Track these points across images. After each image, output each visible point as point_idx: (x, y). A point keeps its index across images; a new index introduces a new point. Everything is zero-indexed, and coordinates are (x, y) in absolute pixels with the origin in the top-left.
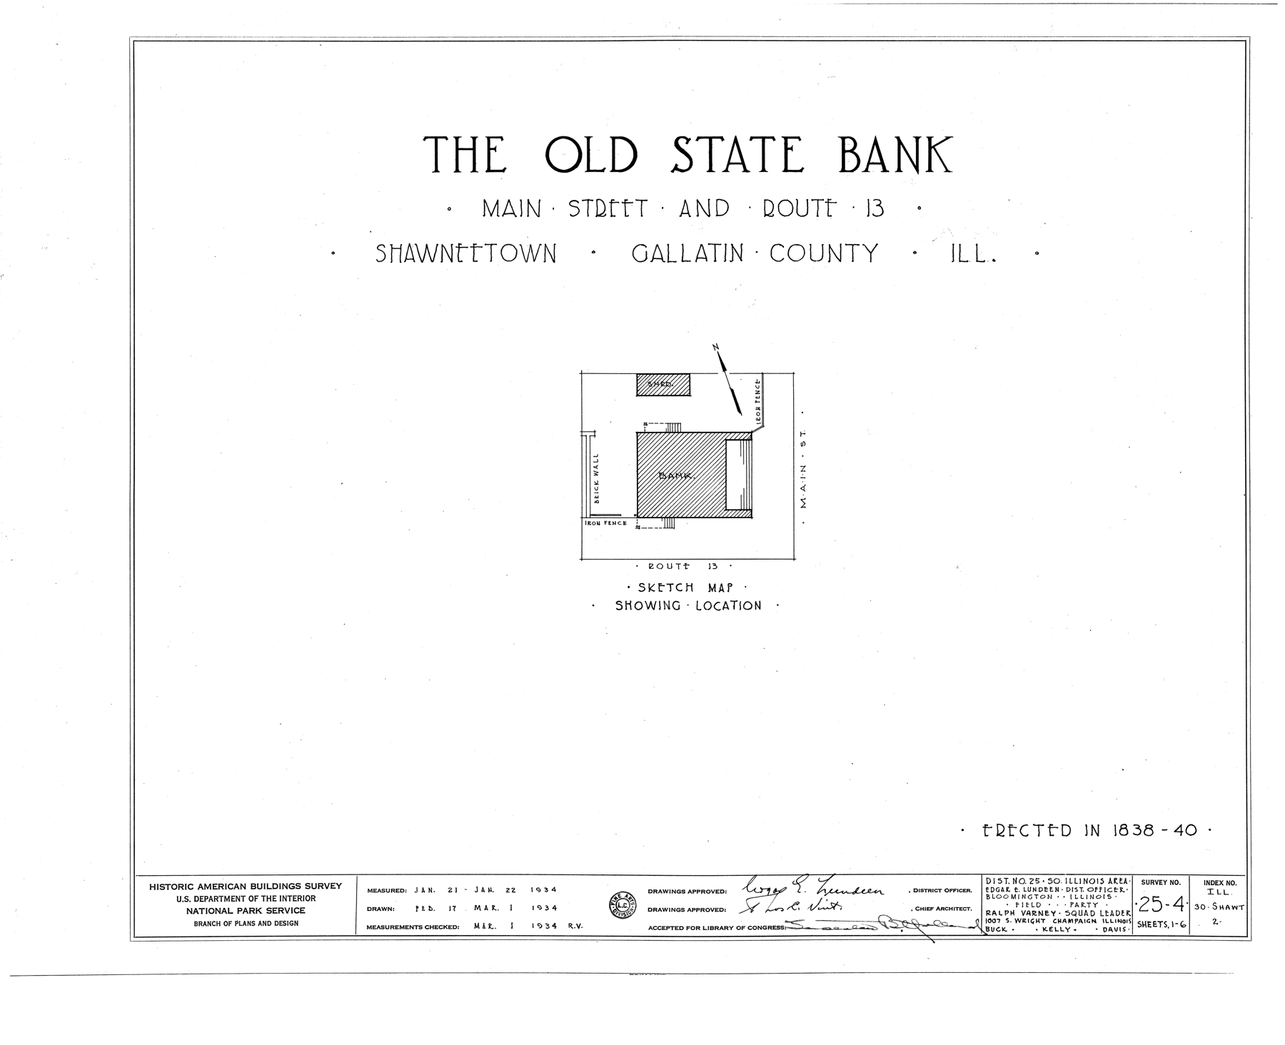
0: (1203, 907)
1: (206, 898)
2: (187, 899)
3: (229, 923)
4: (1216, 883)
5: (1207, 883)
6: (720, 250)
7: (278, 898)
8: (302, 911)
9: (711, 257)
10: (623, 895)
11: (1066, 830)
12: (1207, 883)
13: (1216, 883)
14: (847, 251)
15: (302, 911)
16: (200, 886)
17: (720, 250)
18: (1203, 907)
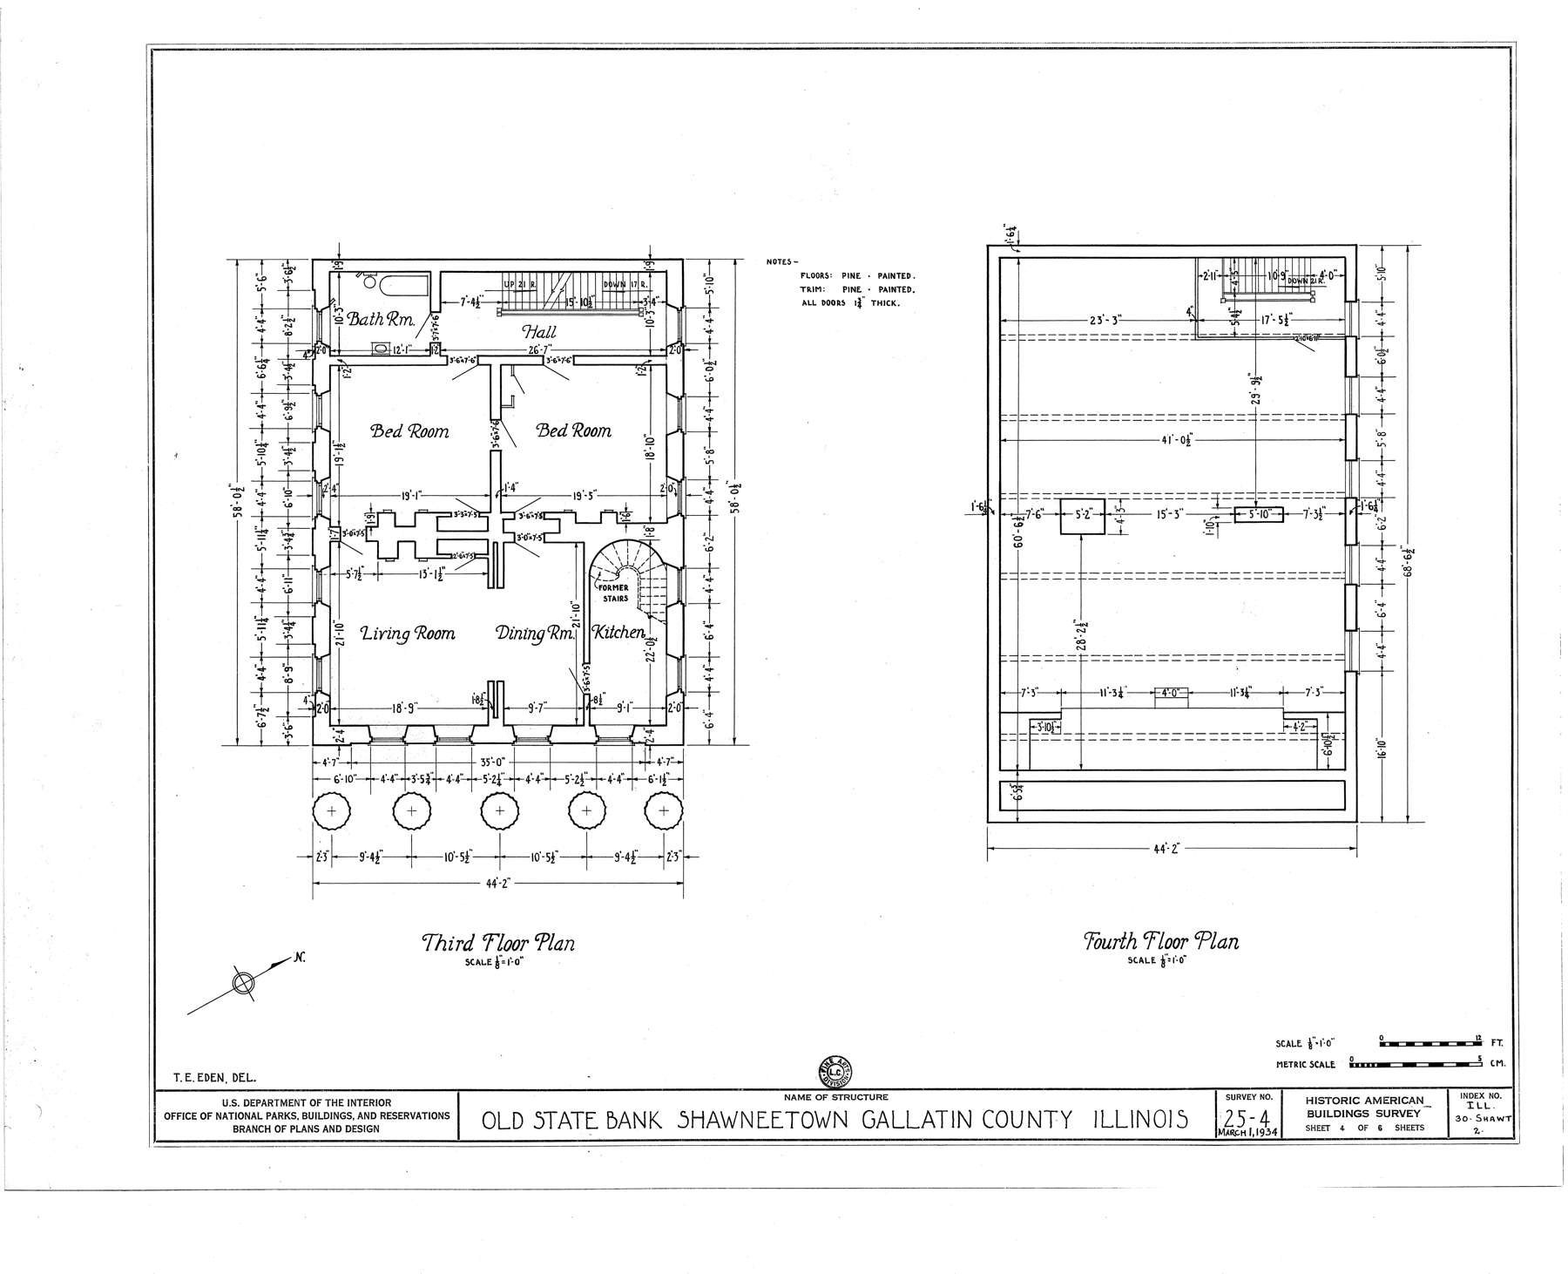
0: (1465, 1119)
1: (258, 1101)
2: (235, 1104)
3: (282, 1128)
4: (1475, 1096)
5: (1465, 1096)
6: (948, 1116)
7: (345, 1103)
8: (1309, 1128)
9: (574, 1124)
10: (835, 1060)
11: (489, 1118)
12: (1465, 1096)
13: (1475, 1096)
14: (1046, 1116)
15: (236, 1129)
16: (1368, 1100)
17: (948, 1116)
18: (1465, 1119)
